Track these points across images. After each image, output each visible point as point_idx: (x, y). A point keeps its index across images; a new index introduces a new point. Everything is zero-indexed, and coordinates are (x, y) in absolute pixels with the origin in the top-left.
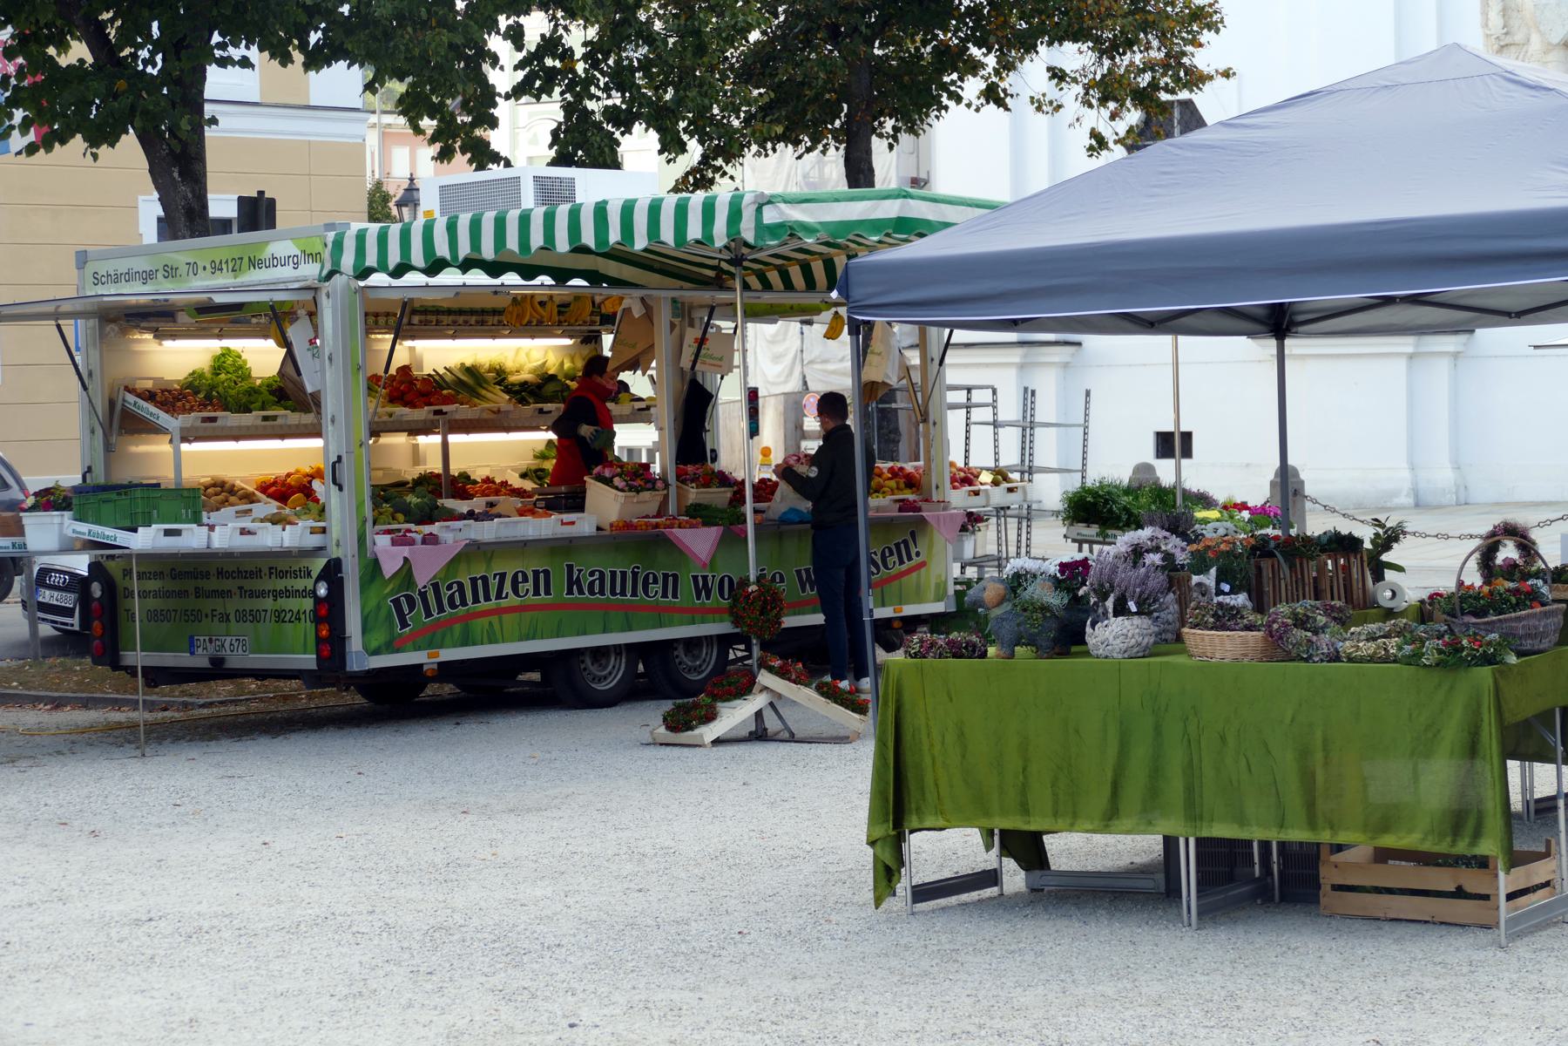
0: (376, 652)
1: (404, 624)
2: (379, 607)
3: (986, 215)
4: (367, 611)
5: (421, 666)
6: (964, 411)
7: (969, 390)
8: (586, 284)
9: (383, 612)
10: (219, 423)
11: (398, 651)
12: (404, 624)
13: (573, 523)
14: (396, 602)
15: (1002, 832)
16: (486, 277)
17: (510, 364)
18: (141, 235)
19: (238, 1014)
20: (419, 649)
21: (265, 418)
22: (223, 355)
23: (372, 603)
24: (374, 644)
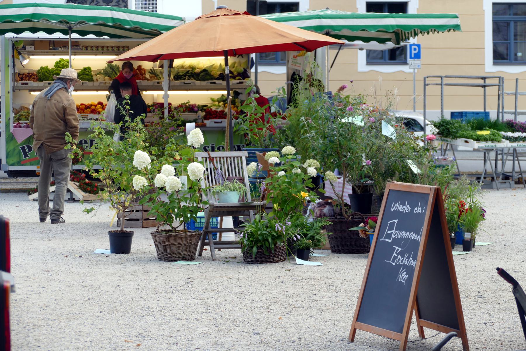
0: (13, 165)
1: (26, 155)
2: (14, 149)
3: (178, 23)
4: (9, 150)
5: (35, 171)
6: (498, 86)
7: (441, 77)
8: (109, 38)
9: (16, 151)
10: (29, 85)
11: (23, 165)
12: (26, 155)
13: (221, 123)
14: (23, 148)
15: (373, 235)
16: (63, 35)
17: (185, 64)
18: (484, 10)
19: (82, 334)
20: (33, 165)
21: (23, 84)
22: (60, 61)
23: (11, 148)
24: (12, 162)
